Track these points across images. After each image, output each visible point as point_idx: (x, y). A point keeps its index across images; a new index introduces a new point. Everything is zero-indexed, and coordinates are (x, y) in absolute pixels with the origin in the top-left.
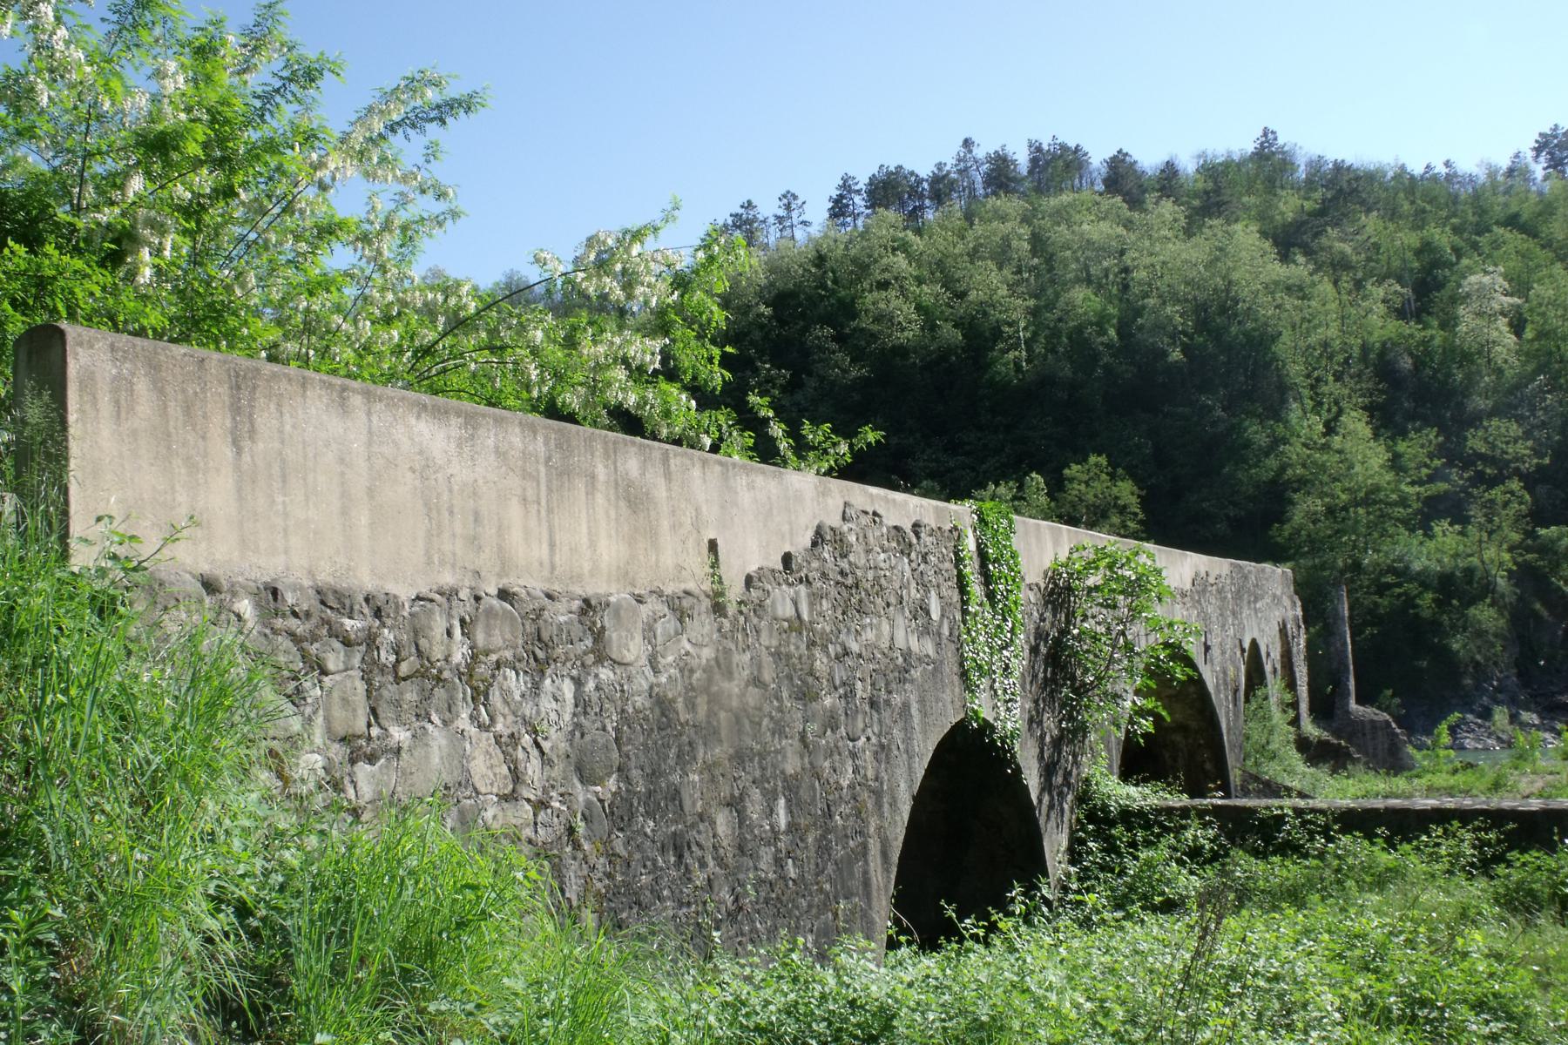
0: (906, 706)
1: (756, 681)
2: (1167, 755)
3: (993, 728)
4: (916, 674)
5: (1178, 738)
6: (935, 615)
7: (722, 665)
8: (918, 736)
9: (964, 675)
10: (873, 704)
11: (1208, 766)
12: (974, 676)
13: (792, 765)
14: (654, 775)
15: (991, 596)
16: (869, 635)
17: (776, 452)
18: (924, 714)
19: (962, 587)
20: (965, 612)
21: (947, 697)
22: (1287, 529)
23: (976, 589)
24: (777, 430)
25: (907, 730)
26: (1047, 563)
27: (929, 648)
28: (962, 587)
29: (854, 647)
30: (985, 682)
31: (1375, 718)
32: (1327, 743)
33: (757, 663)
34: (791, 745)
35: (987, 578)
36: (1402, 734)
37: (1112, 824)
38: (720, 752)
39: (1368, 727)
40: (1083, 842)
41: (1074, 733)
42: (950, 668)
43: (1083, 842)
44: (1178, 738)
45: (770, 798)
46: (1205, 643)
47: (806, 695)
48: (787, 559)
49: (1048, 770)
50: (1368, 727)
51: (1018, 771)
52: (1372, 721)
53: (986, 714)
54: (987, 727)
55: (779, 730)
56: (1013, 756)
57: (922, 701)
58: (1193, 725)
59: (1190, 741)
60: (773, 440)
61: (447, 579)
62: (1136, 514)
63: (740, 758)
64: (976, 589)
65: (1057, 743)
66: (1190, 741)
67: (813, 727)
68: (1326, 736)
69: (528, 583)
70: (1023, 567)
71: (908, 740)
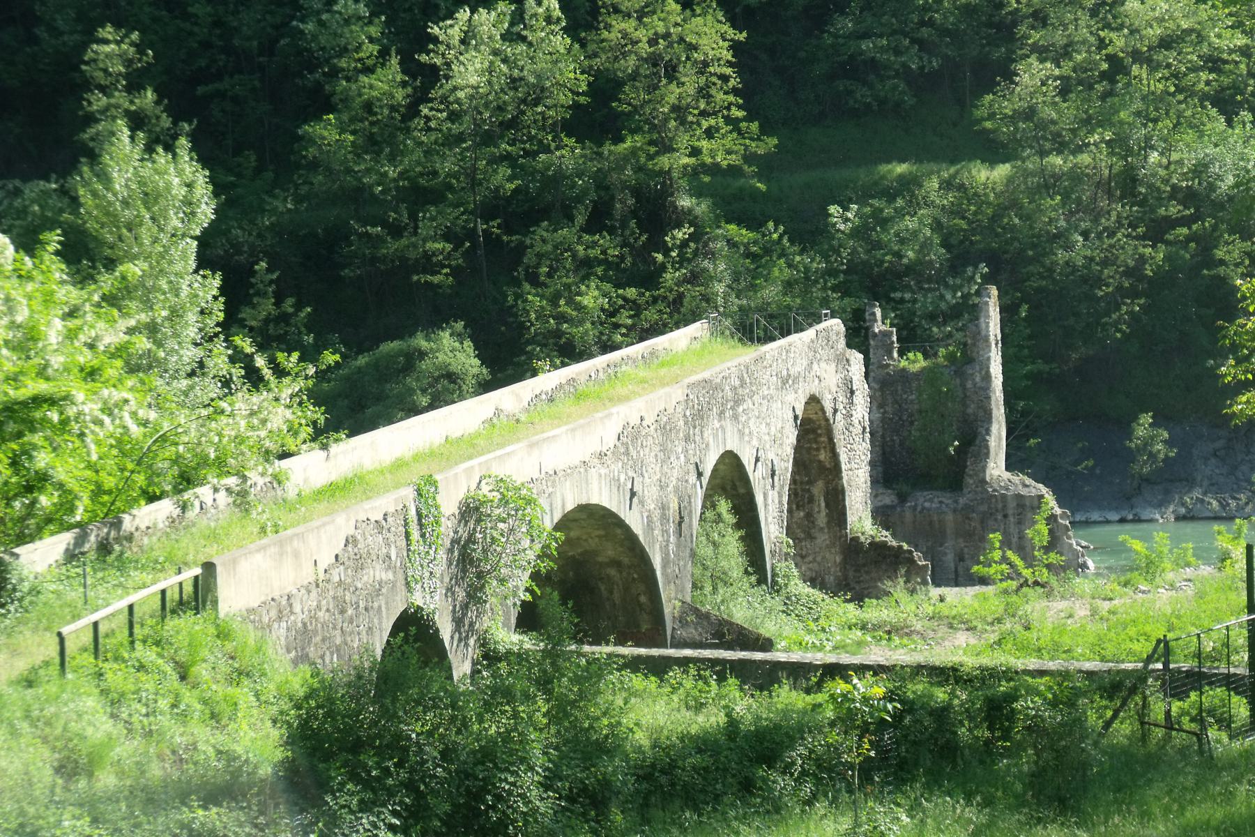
0: (380, 607)
1: (328, 610)
2: (603, 588)
3: (422, 609)
4: (384, 590)
5: (612, 572)
6: (393, 558)
7: (319, 607)
8: (385, 620)
9: (407, 584)
10: (366, 609)
11: (643, 599)
12: (413, 585)
13: (338, 641)
14: (303, 649)
15: (423, 536)
16: (365, 578)
17: (261, 379)
18: (388, 609)
19: (407, 535)
20: (409, 550)
21: (398, 598)
22: (1122, 9)
23: (415, 535)
24: (260, 362)
25: (380, 619)
26: (461, 496)
27: (390, 576)
28: (407, 535)
29: (359, 586)
30: (419, 586)
31: (1024, 492)
32: (883, 546)
33: (328, 603)
34: (338, 632)
35: (421, 525)
36: (1064, 516)
37: (500, 660)
38: (318, 638)
39: (1012, 505)
40: (479, 672)
41: (475, 596)
42: (401, 582)
43: (479, 672)
44: (612, 572)
45: (332, 654)
46: (632, 490)
47: (343, 612)
48: (337, 556)
49: (458, 622)
50: (1012, 505)
51: (437, 630)
52: (1019, 497)
53: (420, 602)
54: (419, 608)
55: (334, 628)
56: (434, 623)
57: (387, 603)
58: (626, 561)
59: (624, 574)
60: (258, 370)
61: (263, 599)
62: (725, 78)
63: (323, 640)
64: (415, 535)
65: (465, 607)
66: (624, 574)
67: (345, 625)
68: (885, 536)
69: (276, 595)
70: (442, 510)
71: (380, 623)
